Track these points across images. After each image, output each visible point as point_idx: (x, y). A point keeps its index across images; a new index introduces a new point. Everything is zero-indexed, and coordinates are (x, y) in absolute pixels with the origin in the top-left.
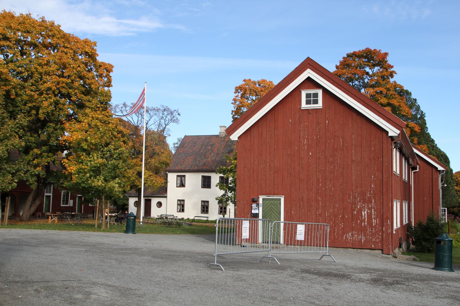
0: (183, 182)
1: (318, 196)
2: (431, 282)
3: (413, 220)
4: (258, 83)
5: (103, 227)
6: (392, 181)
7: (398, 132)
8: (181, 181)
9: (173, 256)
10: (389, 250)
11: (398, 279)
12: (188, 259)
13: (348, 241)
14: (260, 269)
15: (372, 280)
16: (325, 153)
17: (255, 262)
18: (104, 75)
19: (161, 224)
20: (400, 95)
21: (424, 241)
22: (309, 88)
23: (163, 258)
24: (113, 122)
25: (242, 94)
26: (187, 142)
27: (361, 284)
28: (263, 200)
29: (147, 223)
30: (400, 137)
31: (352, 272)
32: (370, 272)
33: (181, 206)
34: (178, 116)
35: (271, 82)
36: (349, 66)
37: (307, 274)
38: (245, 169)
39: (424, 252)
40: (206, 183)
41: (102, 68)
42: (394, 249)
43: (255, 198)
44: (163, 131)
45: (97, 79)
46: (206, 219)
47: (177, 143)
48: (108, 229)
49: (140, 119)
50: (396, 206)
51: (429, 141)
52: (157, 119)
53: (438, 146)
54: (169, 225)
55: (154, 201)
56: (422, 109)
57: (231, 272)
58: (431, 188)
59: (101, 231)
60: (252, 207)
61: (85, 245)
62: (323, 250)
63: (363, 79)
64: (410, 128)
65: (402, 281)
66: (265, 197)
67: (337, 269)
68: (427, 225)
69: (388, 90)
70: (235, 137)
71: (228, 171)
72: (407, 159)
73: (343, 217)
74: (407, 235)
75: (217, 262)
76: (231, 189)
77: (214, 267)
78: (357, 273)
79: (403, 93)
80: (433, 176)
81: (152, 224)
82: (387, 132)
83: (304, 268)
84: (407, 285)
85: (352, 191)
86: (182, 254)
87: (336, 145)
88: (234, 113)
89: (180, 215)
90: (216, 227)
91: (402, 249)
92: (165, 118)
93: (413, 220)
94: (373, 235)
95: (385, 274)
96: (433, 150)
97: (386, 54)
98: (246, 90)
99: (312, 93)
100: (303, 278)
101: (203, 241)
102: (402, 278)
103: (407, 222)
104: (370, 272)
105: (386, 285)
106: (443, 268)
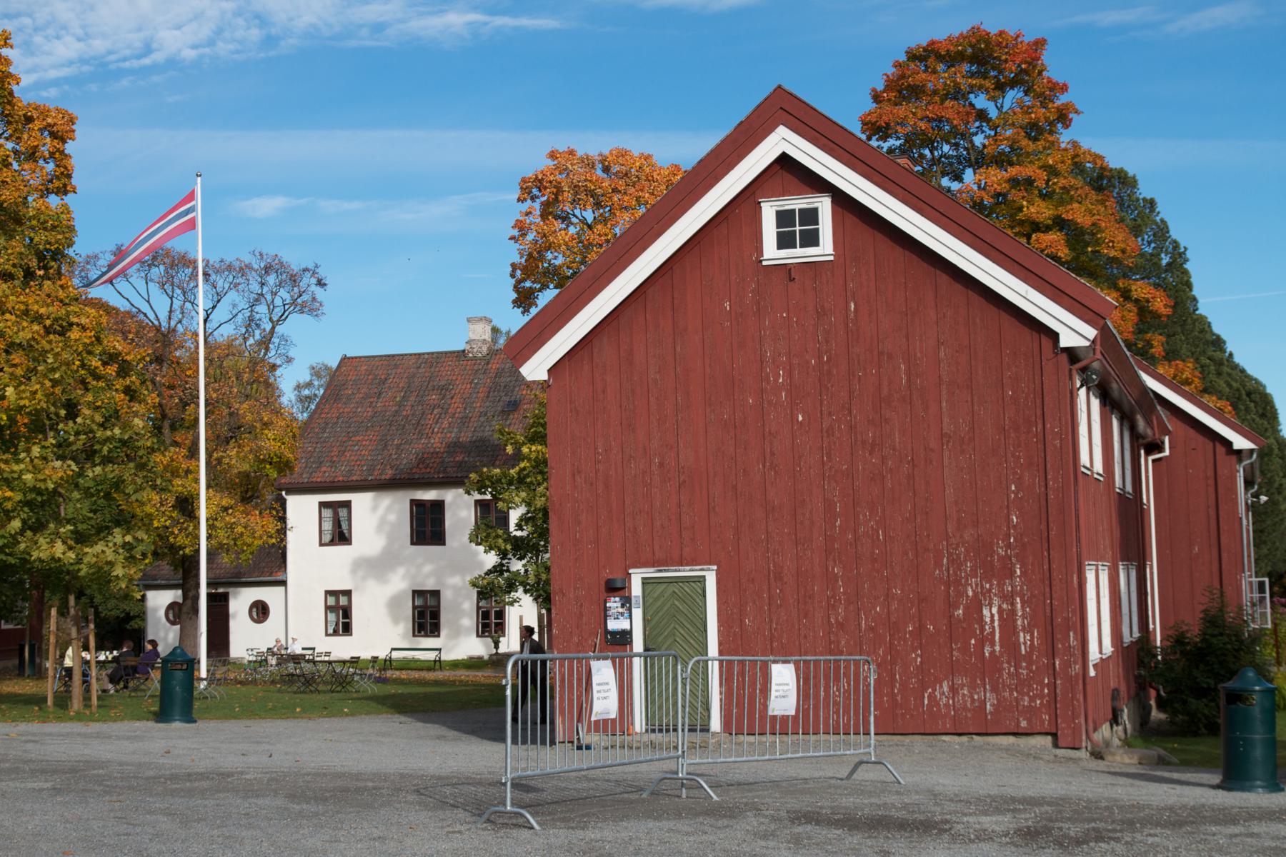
0: (344, 526)
1: (831, 563)
2: (1202, 828)
3: (1156, 626)
4: (602, 162)
5: (76, 704)
6: (1077, 501)
7: (1091, 333)
8: (337, 523)
9: (358, 790)
10: (1076, 732)
11: (1100, 825)
12: (410, 798)
13: (939, 709)
14: (656, 819)
15: (1018, 831)
16: (850, 412)
17: (634, 796)
18: (45, 150)
19: (273, 682)
20: (1099, 189)
21: (1189, 697)
22: (785, 192)
23: (326, 800)
24: (84, 321)
25: (546, 205)
26: (348, 381)
27: (985, 846)
28: (645, 582)
29: (224, 681)
30: (1098, 347)
31: (956, 812)
32: (1014, 810)
33: (341, 614)
34: (318, 291)
35: (648, 157)
36: (915, 92)
37: (809, 827)
38: (577, 477)
39: (1196, 734)
40: (427, 527)
41: (37, 125)
42: (1095, 730)
43: (617, 576)
44: (265, 343)
45: (15, 166)
46: (431, 656)
47: (309, 385)
48: (94, 709)
49: (177, 304)
50: (1097, 584)
51: (1207, 343)
52: (243, 305)
53: (1237, 359)
54: (302, 685)
55: (240, 602)
56: (1175, 233)
57: (562, 833)
58: (1212, 512)
59: (71, 719)
60: (606, 609)
61: (43, 772)
62: (856, 746)
63: (966, 136)
64: (1137, 301)
65: (1114, 831)
66: (651, 573)
67: (905, 807)
68: (1203, 640)
69: (1052, 171)
70: (536, 368)
71: (510, 483)
72: (1128, 420)
73: (921, 628)
74: (1138, 677)
75: (513, 805)
76: (521, 548)
77: (501, 821)
78: (971, 814)
79: (1109, 183)
80: (1219, 472)
81: (241, 683)
82: (1055, 336)
83: (797, 807)
84: (1127, 843)
85: (947, 538)
86: (386, 784)
87: (885, 383)
88: (518, 272)
89: (341, 648)
90: (504, 688)
91: (1120, 728)
92: (269, 297)
93: (1156, 626)
94: (1021, 685)
95: (1060, 812)
96: (1219, 374)
97: (1040, 44)
98: (559, 190)
99: (797, 207)
100: (797, 841)
101: (439, 738)
102: (1113, 822)
103: (1136, 634)
104: (1014, 810)
105: (1061, 845)
106: (1248, 784)
